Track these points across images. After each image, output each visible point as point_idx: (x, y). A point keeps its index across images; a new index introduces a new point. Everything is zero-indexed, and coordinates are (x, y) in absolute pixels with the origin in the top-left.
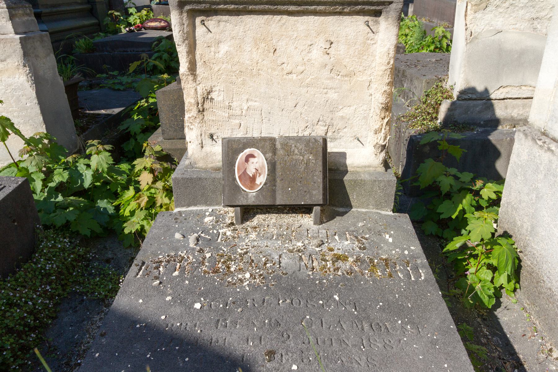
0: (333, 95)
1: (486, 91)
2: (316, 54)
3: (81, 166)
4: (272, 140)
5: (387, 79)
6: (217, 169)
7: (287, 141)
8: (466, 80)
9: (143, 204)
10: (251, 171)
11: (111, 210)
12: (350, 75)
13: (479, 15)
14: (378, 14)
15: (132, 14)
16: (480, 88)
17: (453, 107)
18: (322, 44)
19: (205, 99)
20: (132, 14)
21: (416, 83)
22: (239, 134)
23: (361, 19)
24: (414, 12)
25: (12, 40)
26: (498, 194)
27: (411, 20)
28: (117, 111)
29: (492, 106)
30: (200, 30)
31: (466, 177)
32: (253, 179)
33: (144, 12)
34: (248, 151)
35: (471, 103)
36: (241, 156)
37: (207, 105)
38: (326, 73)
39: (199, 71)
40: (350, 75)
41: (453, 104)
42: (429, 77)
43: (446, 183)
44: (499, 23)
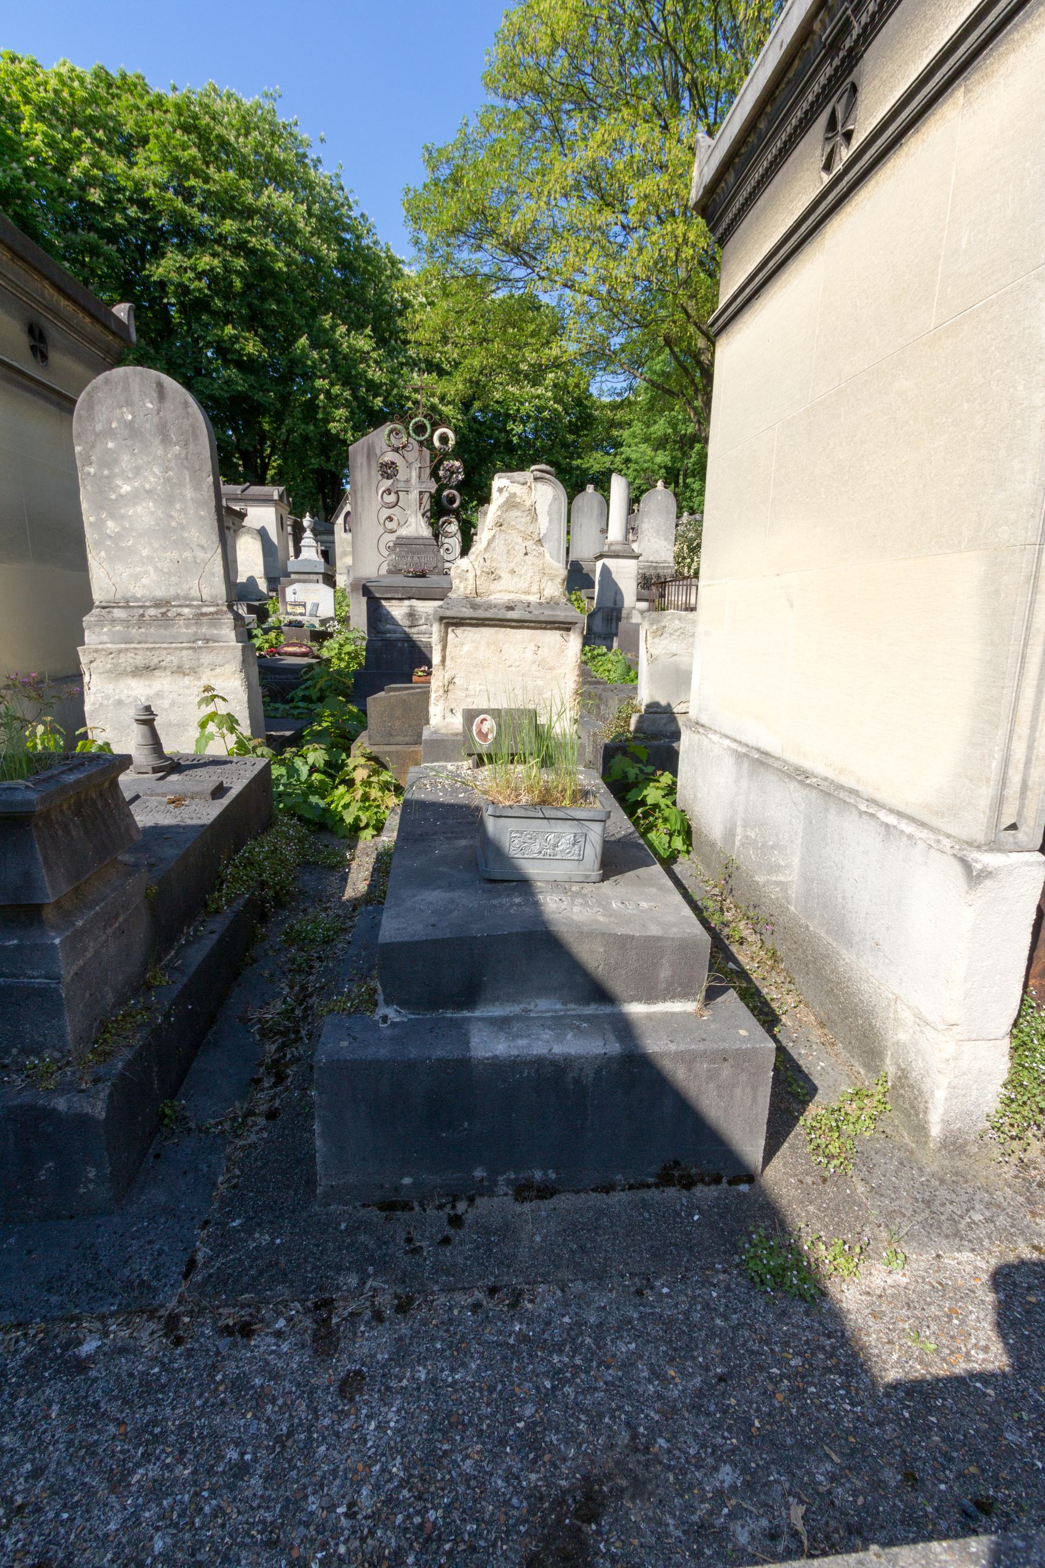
0: (540, 682)
1: (669, 705)
2: (529, 654)
3: (298, 762)
4: (499, 711)
5: (576, 672)
6: (457, 735)
7: (510, 712)
8: (651, 695)
9: (358, 797)
10: (485, 729)
11: (322, 803)
12: (551, 669)
13: (657, 640)
14: (568, 630)
15: (256, 636)
16: (663, 703)
17: (641, 720)
18: (532, 648)
19: (450, 683)
20: (256, 636)
21: (610, 702)
22: (474, 707)
23: (558, 633)
24: (619, 646)
25: (234, 648)
26: (674, 783)
27: (615, 654)
28: (288, 733)
29: (675, 719)
30: (451, 636)
31: (649, 769)
32: (486, 735)
33: (272, 635)
34: (482, 717)
35: (657, 716)
36: (478, 720)
37: (451, 687)
38: (535, 667)
39: (447, 662)
40: (551, 669)
41: (641, 716)
42: (622, 695)
43: (633, 772)
44: (674, 647)
